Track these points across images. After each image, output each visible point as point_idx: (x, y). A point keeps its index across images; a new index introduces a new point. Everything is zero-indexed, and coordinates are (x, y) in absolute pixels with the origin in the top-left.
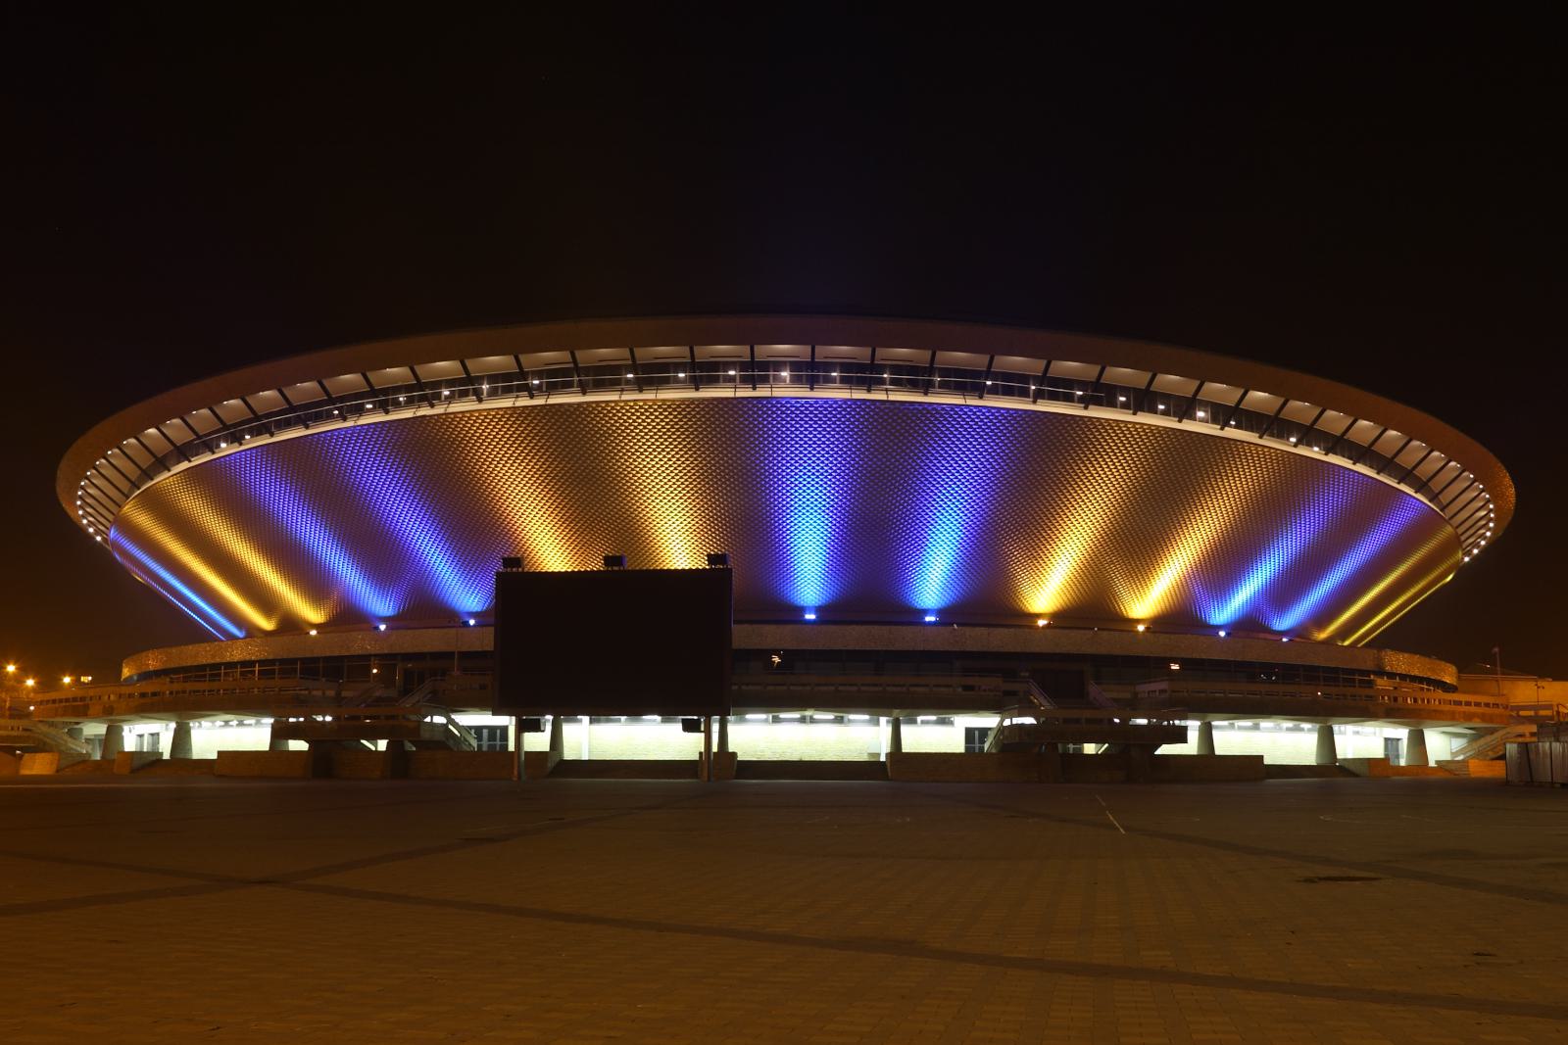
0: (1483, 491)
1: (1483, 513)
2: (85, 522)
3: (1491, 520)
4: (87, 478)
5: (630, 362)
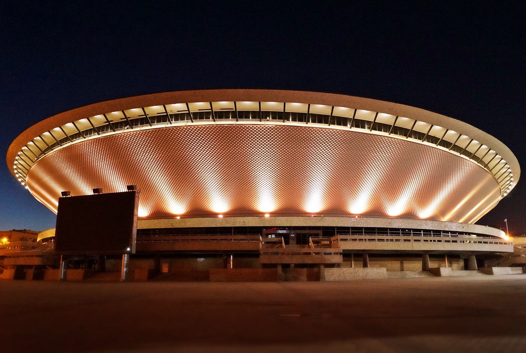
4: (18, 156)
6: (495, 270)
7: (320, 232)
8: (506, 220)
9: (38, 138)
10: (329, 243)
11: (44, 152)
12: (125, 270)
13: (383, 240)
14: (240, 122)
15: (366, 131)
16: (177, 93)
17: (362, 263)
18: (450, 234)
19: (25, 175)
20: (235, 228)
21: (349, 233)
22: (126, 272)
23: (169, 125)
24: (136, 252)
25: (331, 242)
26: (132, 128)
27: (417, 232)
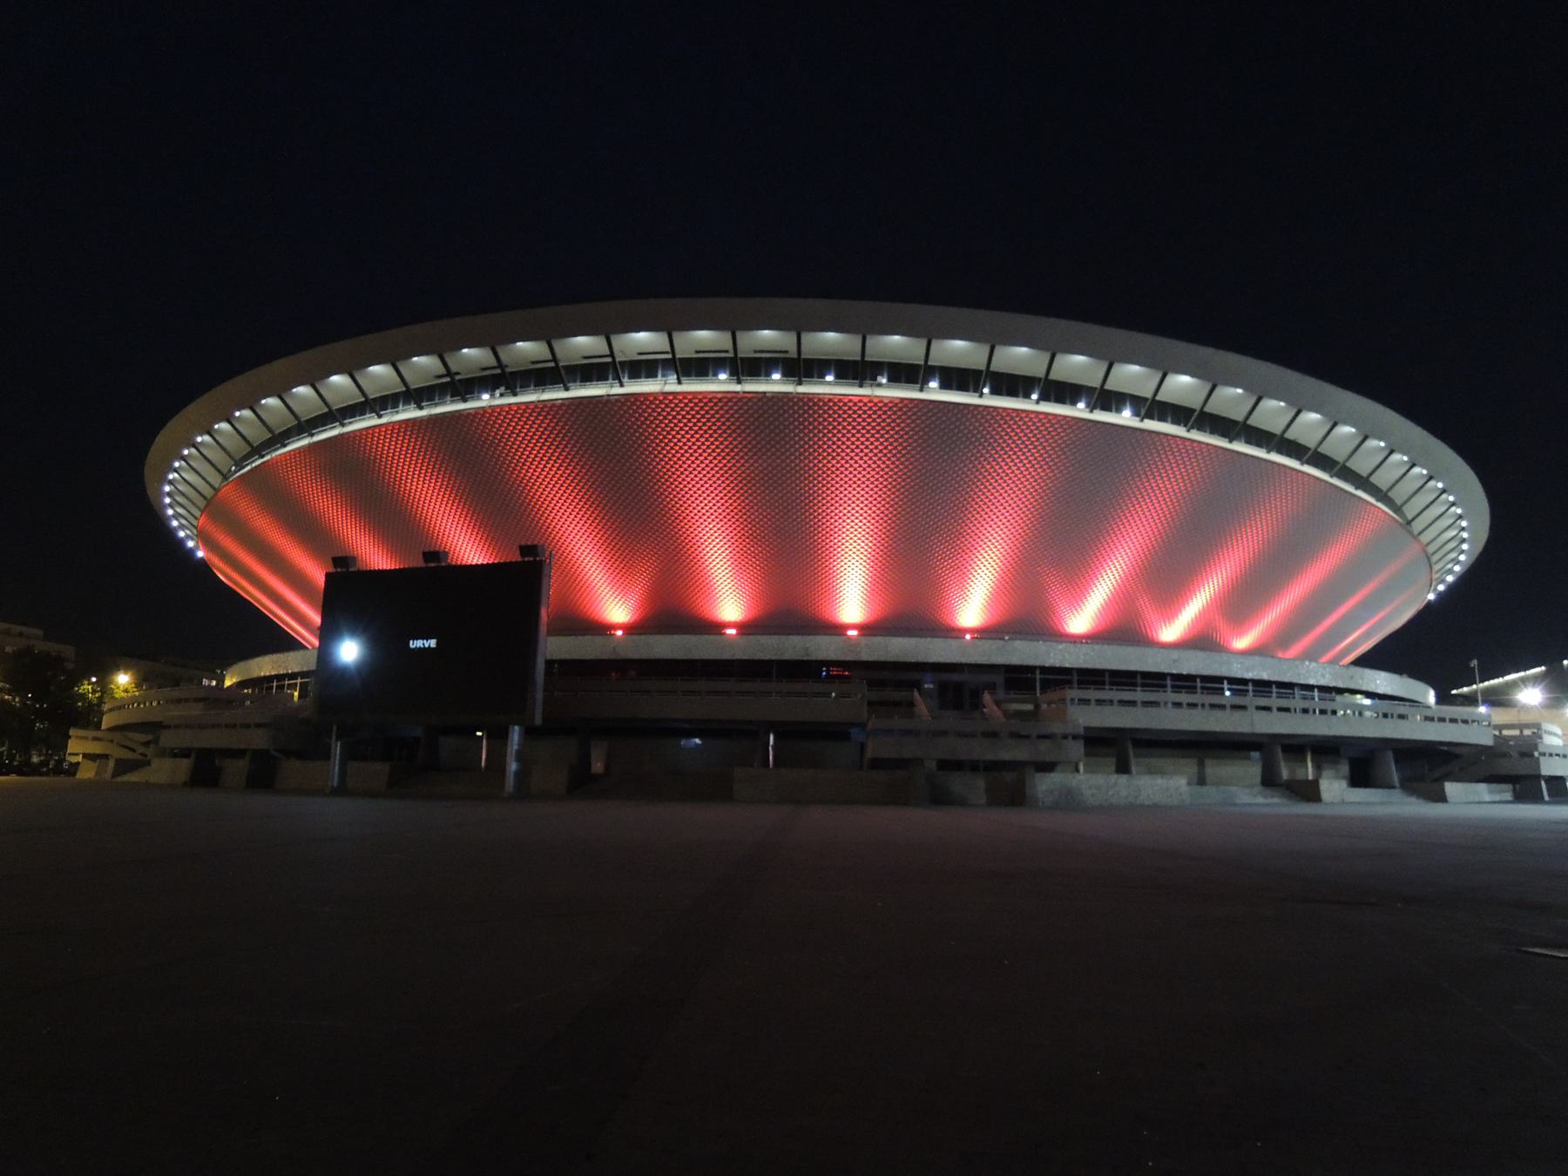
0: (1444, 491)
1: (1453, 533)
2: (170, 512)
3: (1463, 541)
4: (183, 458)
5: (731, 355)
6: (1451, 788)
7: (999, 679)
8: (1474, 663)
10: (1030, 707)
11: (257, 450)
12: (513, 767)
13: (1132, 703)
14: (1150, 425)
15: (1126, 417)
17: (1112, 761)
18: (1316, 693)
19: (198, 513)
21: (1164, 686)
22: (517, 773)
23: (617, 390)
24: (544, 719)
25: (1037, 706)
26: (515, 394)
27: (1154, 680)
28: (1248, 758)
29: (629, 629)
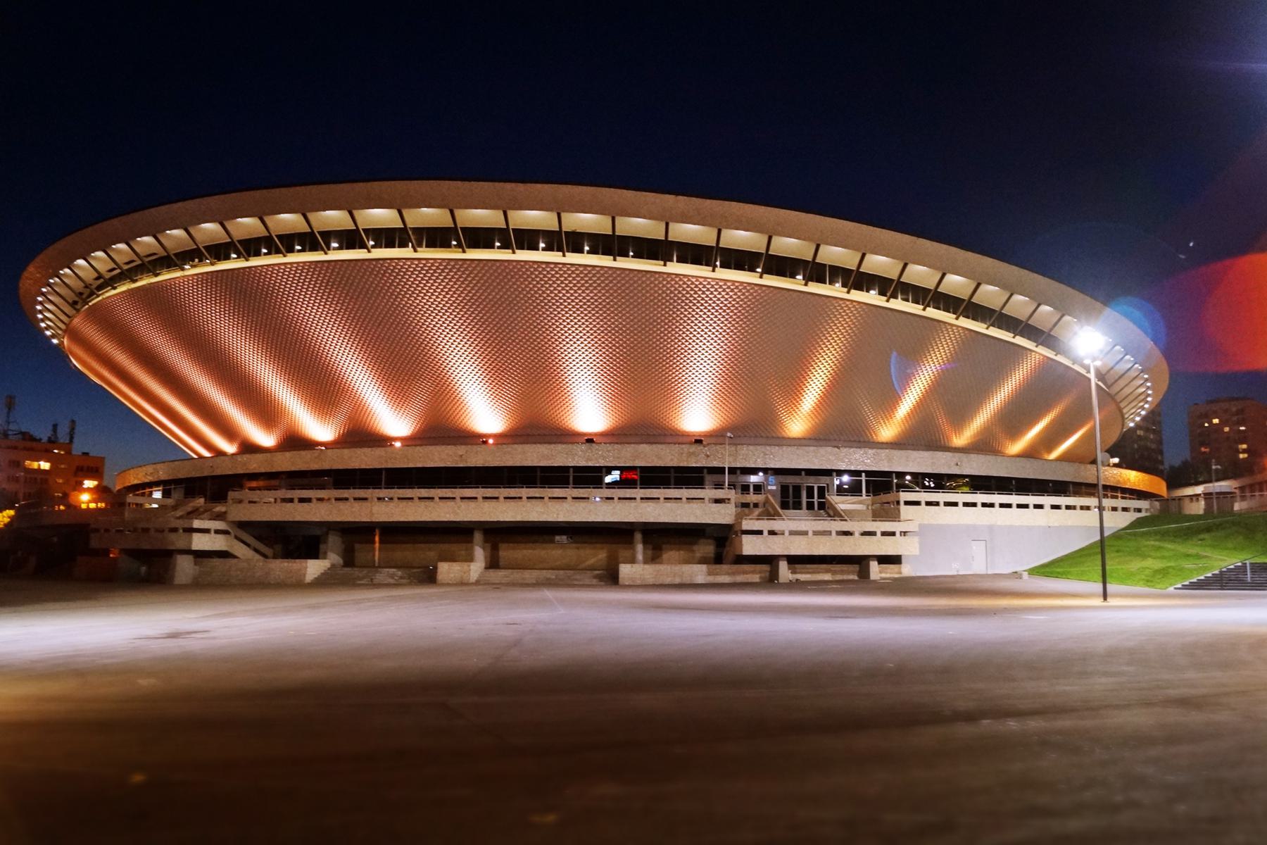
3: (1149, 395)
4: (49, 285)
9: (67, 271)
13: (308, 500)
16: (377, 187)
20: (388, 470)
28: (553, 542)
29: (409, 441)
